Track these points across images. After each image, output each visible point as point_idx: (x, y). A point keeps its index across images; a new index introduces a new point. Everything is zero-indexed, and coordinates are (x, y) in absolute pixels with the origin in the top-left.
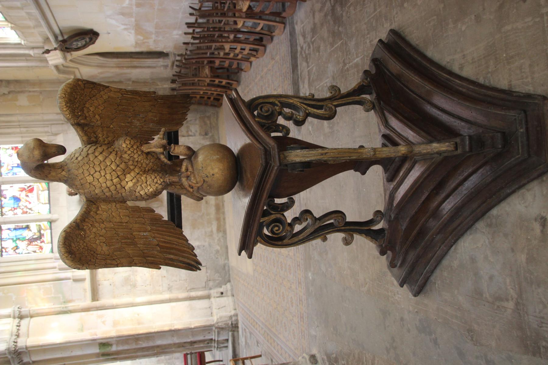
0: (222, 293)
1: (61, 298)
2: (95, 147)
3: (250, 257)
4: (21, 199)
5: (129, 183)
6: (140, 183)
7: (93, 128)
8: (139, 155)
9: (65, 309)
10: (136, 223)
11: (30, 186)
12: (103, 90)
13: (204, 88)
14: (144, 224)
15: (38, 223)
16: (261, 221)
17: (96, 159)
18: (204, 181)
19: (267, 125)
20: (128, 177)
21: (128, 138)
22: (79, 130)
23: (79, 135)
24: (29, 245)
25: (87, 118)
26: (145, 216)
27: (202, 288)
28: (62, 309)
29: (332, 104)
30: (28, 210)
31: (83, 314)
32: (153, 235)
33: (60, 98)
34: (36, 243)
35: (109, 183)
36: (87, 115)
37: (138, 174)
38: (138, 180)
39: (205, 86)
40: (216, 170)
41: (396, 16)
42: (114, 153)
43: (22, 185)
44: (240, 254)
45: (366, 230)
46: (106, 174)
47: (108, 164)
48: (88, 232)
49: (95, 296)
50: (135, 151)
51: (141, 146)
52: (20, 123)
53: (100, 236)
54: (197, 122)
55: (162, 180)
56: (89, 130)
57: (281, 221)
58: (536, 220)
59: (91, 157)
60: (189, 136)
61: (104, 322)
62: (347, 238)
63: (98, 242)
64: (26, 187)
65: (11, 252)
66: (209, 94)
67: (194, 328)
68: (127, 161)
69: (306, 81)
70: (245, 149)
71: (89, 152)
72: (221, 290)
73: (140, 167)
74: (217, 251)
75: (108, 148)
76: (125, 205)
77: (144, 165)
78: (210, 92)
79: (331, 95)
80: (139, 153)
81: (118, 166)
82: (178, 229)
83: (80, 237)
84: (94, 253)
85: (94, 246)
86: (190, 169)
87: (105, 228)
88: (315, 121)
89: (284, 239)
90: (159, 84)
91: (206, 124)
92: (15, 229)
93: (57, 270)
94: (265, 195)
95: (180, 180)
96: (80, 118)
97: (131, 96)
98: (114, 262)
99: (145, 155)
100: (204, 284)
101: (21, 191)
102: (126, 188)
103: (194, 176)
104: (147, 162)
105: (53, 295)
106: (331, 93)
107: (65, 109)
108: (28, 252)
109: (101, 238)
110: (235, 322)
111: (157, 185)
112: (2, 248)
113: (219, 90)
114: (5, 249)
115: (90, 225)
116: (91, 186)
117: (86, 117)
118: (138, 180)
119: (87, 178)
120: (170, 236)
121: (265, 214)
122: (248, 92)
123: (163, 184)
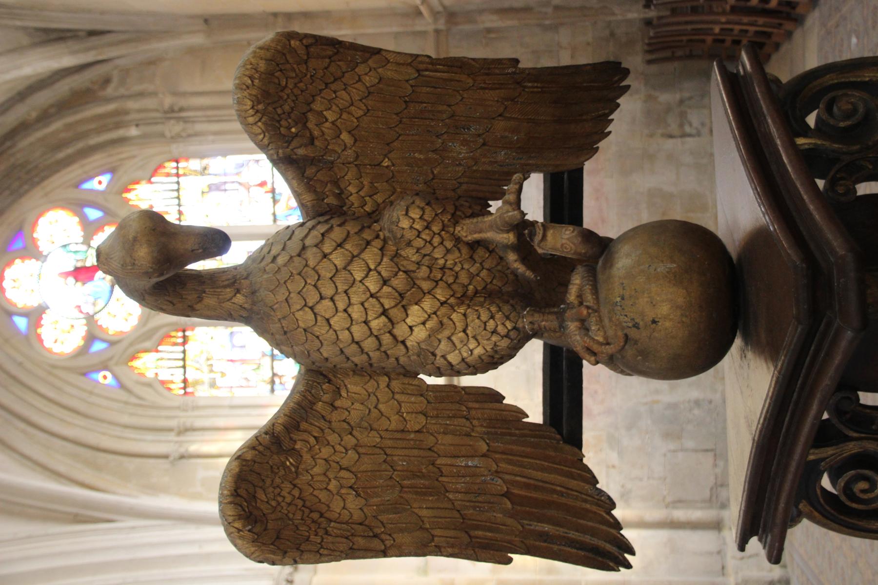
3: (775, 557)
5: (416, 325)
6: (447, 333)
7: (330, 169)
8: (448, 251)
10: (445, 433)
13: (723, 19)
14: (468, 435)
16: (811, 457)
17: (325, 263)
18: (626, 337)
20: (415, 314)
21: (418, 202)
22: (290, 175)
25: (317, 143)
26: (473, 412)
27: (704, 501)
32: (494, 467)
35: (358, 331)
36: (316, 133)
37: (442, 304)
38: (441, 323)
39: (724, 13)
40: (664, 309)
44: (742, 548)
46: (350, 304)
47: (358, 276)
48: (307, 457)
50: (436, 240)
51: (456, 223)
53: (341, 469)
55: (509, 325)
56: (319, 176)
59: (312, 256)
60: (684, 135)
66: (736, 32)
68: (412, 267)
70: (758, 239)
71: (308, 242)
76: (416, 382)
77: (464, 278)
78: (737, 28)
80: (449, 244)
81: (385, 282)
82: (568, 447)
83: (282, 472)
84: (322, 515)
85: (323, 496)
87: (355, 448)
90: (616, 9)
94: (827, 381)
95: (562, 326)
96: (294, 144)
99: (465, 250)
100: (707, 494)
103: (600, 320)
107: (251, 120)
109: (344, 474)
112: (274, 375)
113: (761, 20)
114: (280, 377)
115: (312, 441)
116: (309, 335)
118: (441, 323)
119: (299, 315)
120: (543, 469)
121: (824, 436)
122: (837, 26)
123: (513, 334)
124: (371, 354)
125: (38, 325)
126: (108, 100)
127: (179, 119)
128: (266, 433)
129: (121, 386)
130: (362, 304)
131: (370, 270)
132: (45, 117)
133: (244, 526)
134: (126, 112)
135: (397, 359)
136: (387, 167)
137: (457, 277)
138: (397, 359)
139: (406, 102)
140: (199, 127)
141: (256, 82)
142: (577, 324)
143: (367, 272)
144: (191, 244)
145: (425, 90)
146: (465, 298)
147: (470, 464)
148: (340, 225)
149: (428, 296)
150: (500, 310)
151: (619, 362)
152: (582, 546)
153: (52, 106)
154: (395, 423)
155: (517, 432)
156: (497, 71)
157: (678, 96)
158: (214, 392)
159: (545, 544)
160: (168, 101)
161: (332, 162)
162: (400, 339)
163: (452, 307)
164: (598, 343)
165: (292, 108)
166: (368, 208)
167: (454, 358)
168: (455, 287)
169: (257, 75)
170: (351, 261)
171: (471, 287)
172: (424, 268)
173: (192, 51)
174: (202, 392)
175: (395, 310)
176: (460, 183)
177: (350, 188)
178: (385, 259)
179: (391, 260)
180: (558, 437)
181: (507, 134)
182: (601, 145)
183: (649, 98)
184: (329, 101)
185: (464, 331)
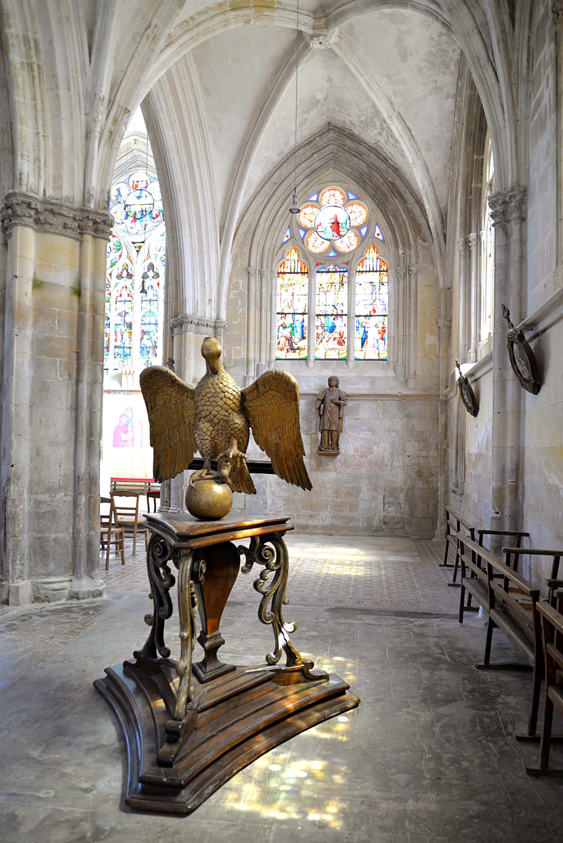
15: (306, 348)
24: (286, 338)
30: (319, 340)
34: (287, 345)
35: (201, 408)
43: (345, 335)
54: (399, 515)
58: (93, 785)
63: (165, 397)
65: (281, 322)
71: (226, 394)
91: (396, 523)
92: (303, 326)
125: (312, 206)
126: (415, 241)
127: (405, 273)
129: (283, 244)
132: (408, 211)
134: (410, 249)
140: (401, 282)
153: (414, 215)
158: (279, 286)
160: (414, 269)
173: (437, 280)
174: (280, 281)
183: (402, 490)
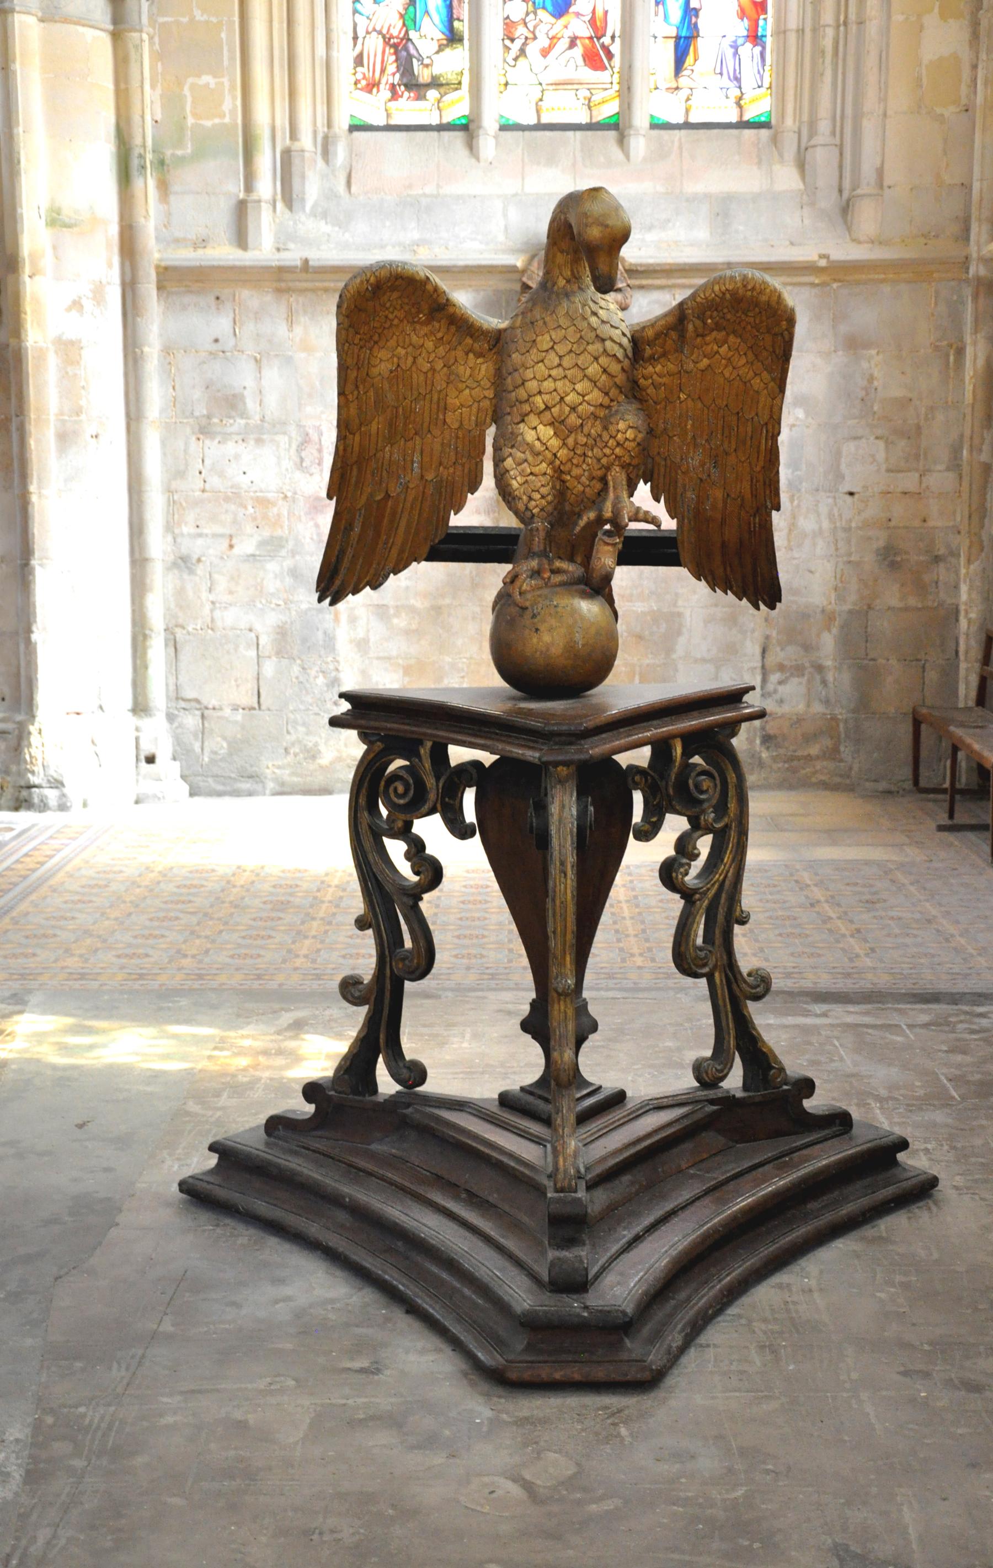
0: (151, 760)
1: (179, 153)
2: (620, 354)
3: (335, 722)
4: (564, 20)
6: (530, 458)
8: (599, 460)
9: (135, 162)
10: (442, 444)
11: (610, 56)
12: (773, 380)
14: (441, 464)
19: (662, 784)
20: (546, 432)
21: (640, 436)
23: (658, 319)
24: (387, 40)
25: (699, 339)
26: (460, 468)
28: (136, 151)
29: (715, 967)
31: (114, 230)
32: (411, 486)
33: (745, 277)
34: (391, 68)
35: (532, 385)
36: (708, 338)
37: (555, 455)
40: (547, 638)
41: (977, 1197)
42: (606, 401)
43: (614, 25)
44: (342, 696)
45: (378, 1038)
46: (555, 380)
47: (579, 387)
49: (175, 280)
51: (623, 467)
52: (853, 28)
53: (415, 358)
57: (417, 804)
59: (596, 348)
61: (77, 305)
62: (361, 987)
63: (401, 351)
64: (606, 40)
67: (28, 641)
68: (586, 430)
69: (867, 1020)
72: (163, 757)
73: (570, 460)
74: (313, 754)
75: (617, 386)
76: (488, 420)
77: (576, 472)
79: (745, 974)
80: (604, 461)
84: (376, 343)
85: (392, 343)
86: (557, 579)
88: (706, 992)
89: (370, 813)
91: (809, 739)
93: (283, 141)
96: (698, 323)
97: (763, 447)
98: (350, 387)
99: (599, 473)
101: (593, 22)
102: (522, 425)
104: (584, 479)
105: (190, 121)
106: (750, 975)
107: (716, 288)
108: (361, 33)
109: (410, 359)
110: (36, 800)
111: (525, 498)
115: (439, 335)
116: (529, 345)
117: (703, 336)
119: (547, 337)
123: (528, 514)
124: (514, 394)
128: (448, 300)
130: (555, 390)
131: (583, 396)
133: (371, 285)
135: (509, 414)
136: (679, 398)
137: (577, 466)
138: (509, 414)
139: (738, 413)
141: (749, 293)
142: (536, 567)
143: (583, 395)
144: (603, 267)
145: (749, 429)
146: (559, 473)
147: (415, 465)
148: (623, 369)
149: (561, 443)
150: (549, 503)
151: (503, 601)
152: (339, 560)
154: (453, 401)
155: (442, 506)
156: (768, 492)
157: (829, 663)
159: (342, 527)
161: (682, 352)
162: (526, 418)
163: (551, 463)
164: (521, 586)
165: (728, 320)
166: (642, 381)
167: (509, 463)
168: (569, 464)
169: (755, 293)
170: (591, 380)
171: (568, 477)
172: (585, 440)
175: (550, 416)
176: (665, 459)
177: (659, 366)
178: (592, 408)
179: (592, 413)
180: (437, 541)
181: (711, 500)
182: (703, 583)
184: (737, 349)
185: (531, 473)
